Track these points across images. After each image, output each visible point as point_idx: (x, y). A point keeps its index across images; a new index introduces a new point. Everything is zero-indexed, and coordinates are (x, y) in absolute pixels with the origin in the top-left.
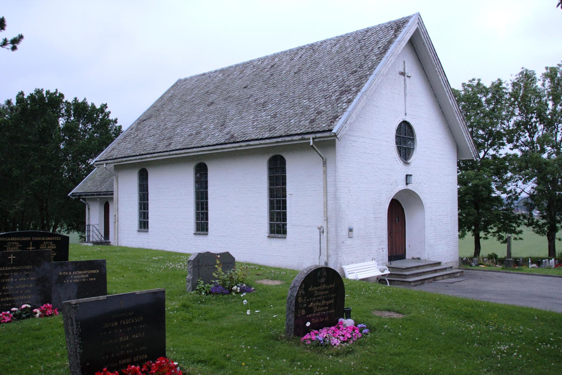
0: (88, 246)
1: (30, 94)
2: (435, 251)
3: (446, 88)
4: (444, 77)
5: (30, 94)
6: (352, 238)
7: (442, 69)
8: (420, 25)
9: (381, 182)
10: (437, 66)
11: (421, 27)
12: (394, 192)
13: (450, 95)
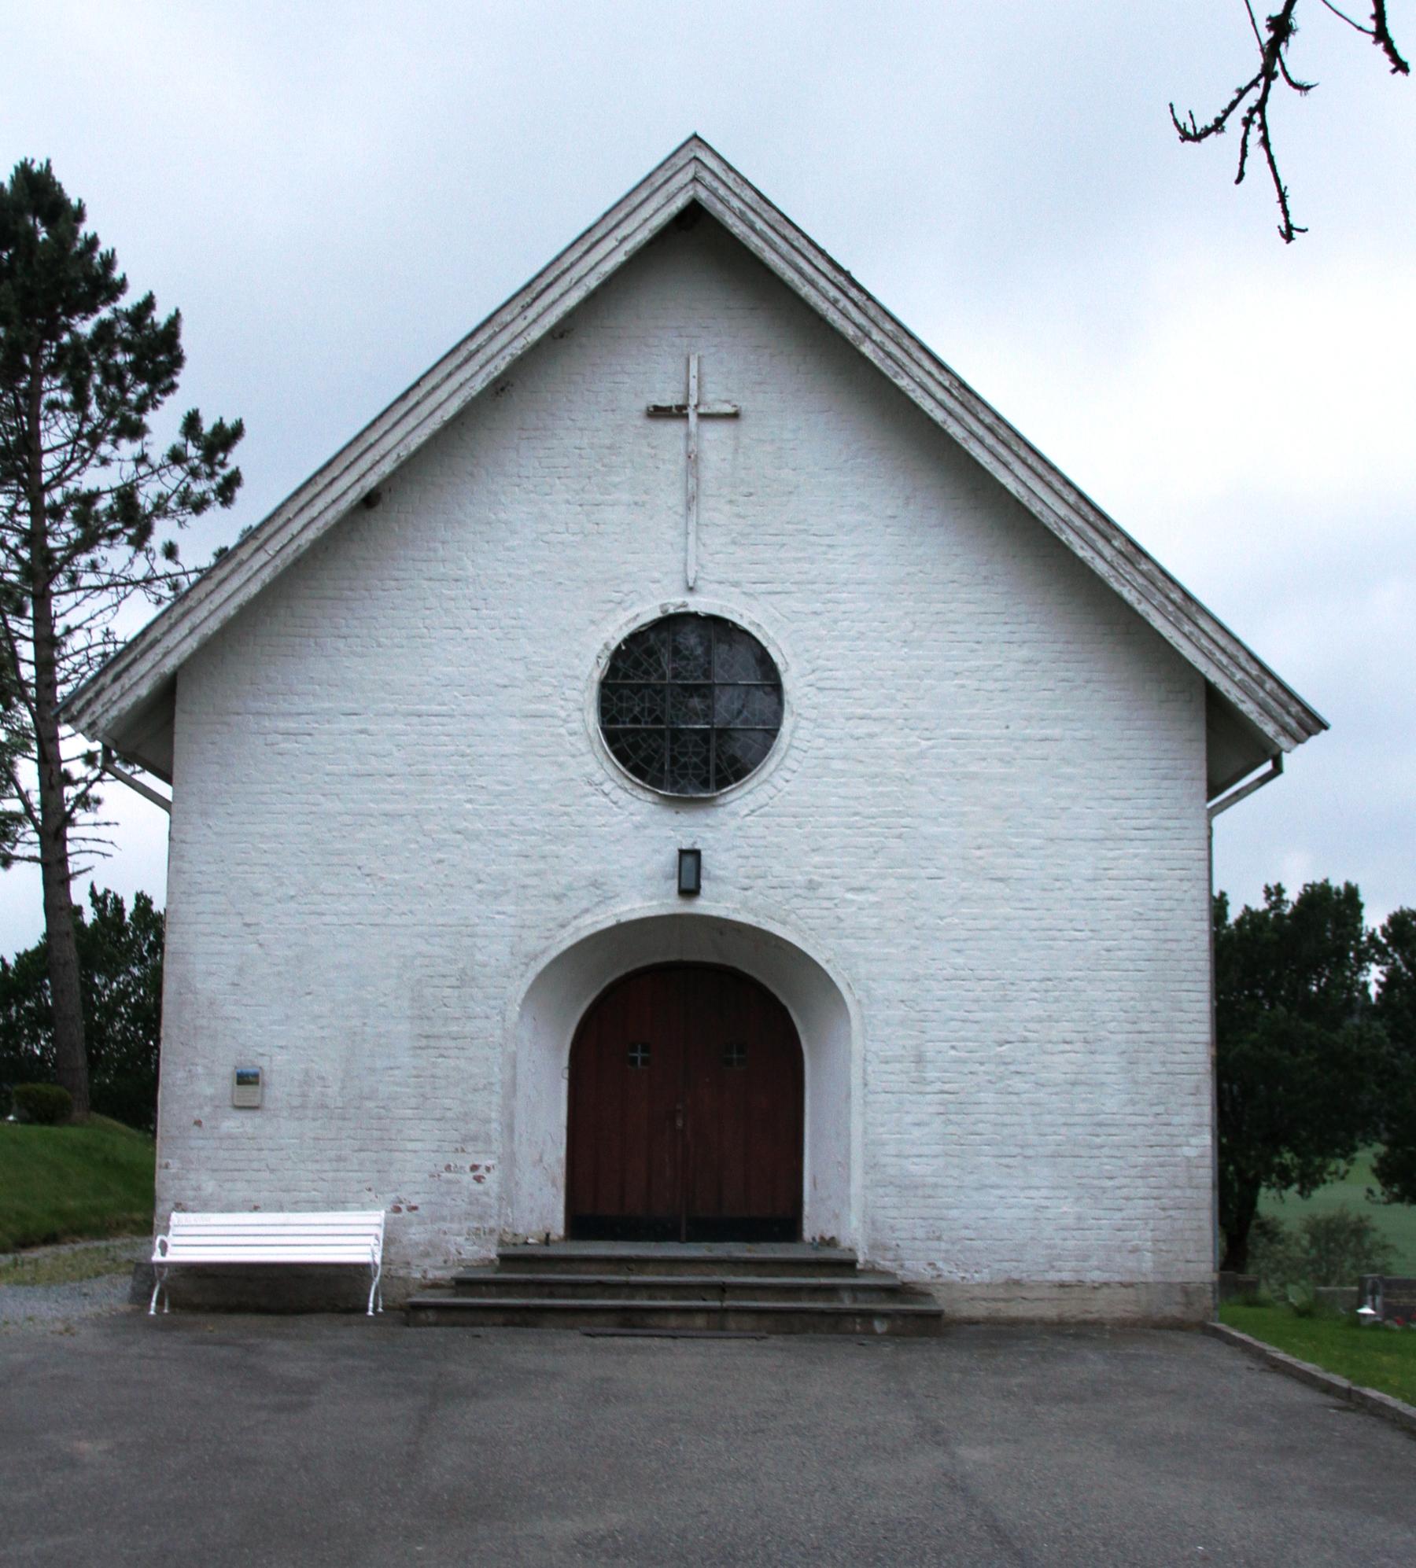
0: (1405, 1400)
1: (1347, 885)
2: (954, 1213)
3: (959, 420)
4: (930, 374)
5: (1347, 885)
6: (258, 1113)
7: (906, 342)
8: (716, 184)
9: (479, 887)
10: (868, 335)
11: (722, 191)
12: (578, 929)
13: (1002, 450)
